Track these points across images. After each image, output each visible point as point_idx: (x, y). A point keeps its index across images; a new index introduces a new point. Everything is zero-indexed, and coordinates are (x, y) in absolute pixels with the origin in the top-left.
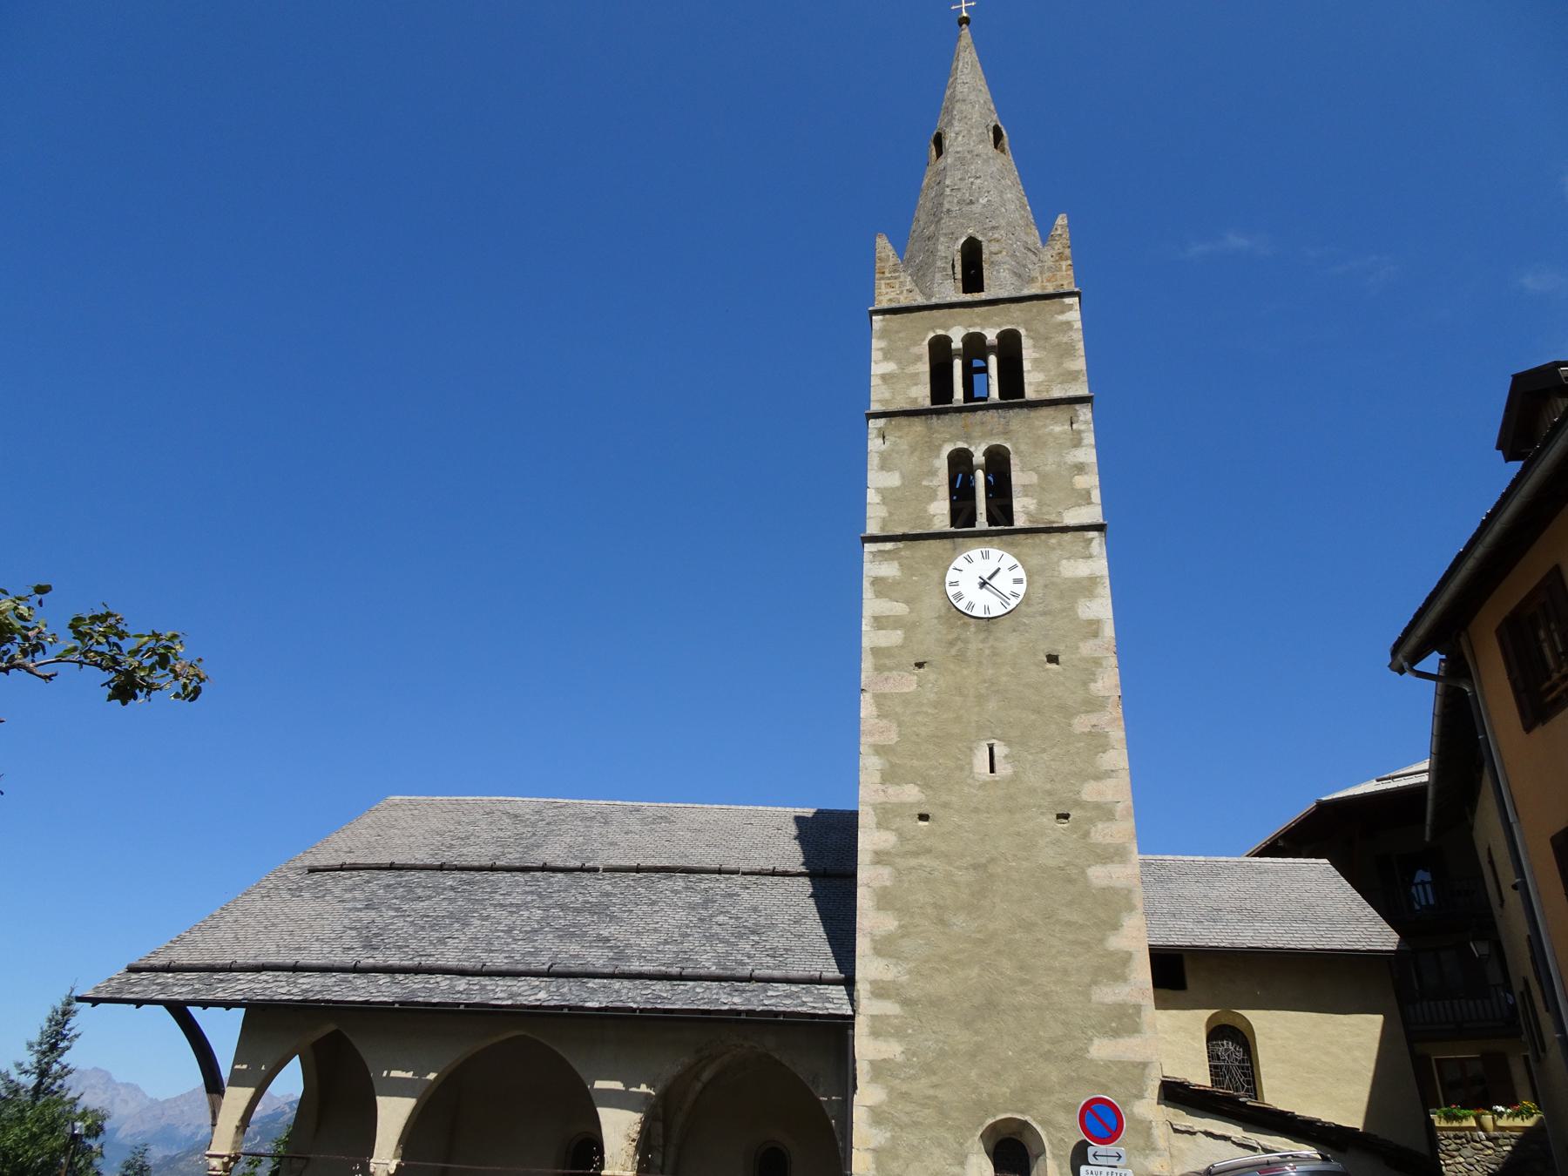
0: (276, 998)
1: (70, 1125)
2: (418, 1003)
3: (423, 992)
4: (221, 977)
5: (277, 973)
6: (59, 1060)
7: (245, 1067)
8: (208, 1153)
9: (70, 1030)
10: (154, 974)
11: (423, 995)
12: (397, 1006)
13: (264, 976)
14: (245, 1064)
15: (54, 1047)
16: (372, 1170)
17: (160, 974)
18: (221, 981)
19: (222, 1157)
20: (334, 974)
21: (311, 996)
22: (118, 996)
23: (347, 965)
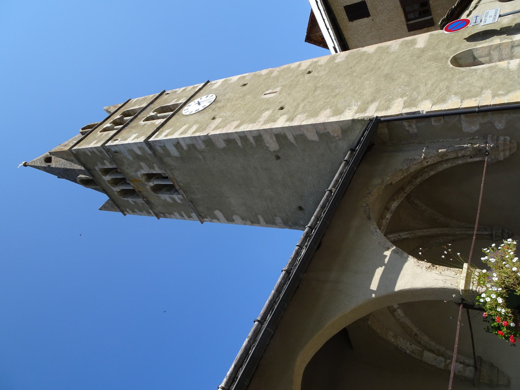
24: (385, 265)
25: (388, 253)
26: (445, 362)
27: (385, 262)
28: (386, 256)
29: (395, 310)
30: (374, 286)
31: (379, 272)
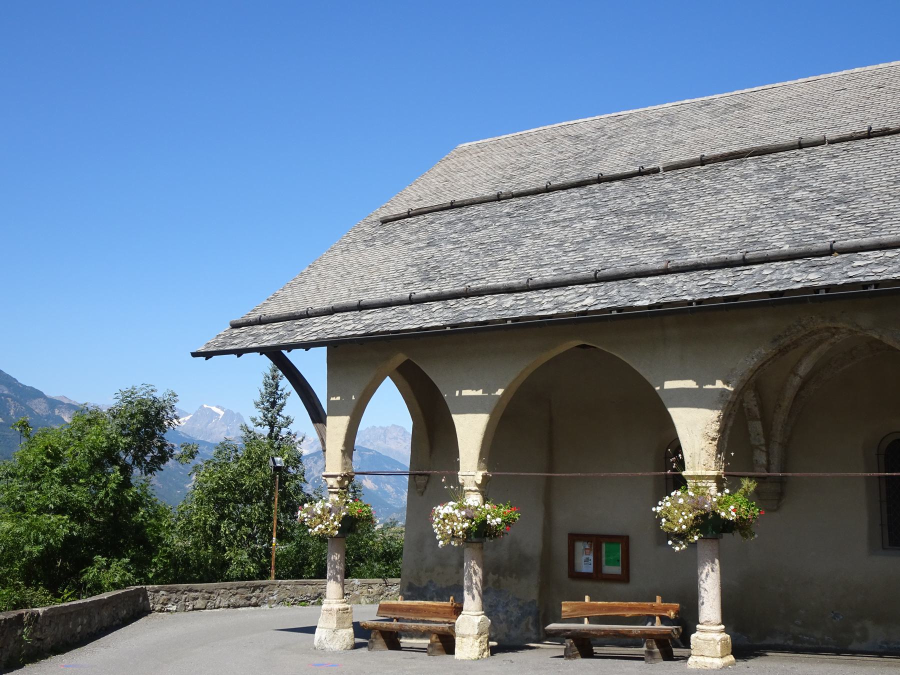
0: (343, 335)
2: (467, 324)
3: (472, 313)
4: (301, 323)
6: (280, 413)
7: (338, 398)
8: (324, 473)
9: (282, 390)
10: (251, 327)
11: (472, 316)
12: (448, 329)
13: (335, 318)
15: (273, 404)
16: (461, 481)
17: (255, 327)
18: (301, 326)
20: (393, 308)
21: (372, 330)
22: (221, 349)
24: (701, 387)
25: (719, 384)
26: (761, 445)
27: (705, 386)
28: (714, 384)
29: (796, 374)
30: (669, 385)
31: (690, 384)
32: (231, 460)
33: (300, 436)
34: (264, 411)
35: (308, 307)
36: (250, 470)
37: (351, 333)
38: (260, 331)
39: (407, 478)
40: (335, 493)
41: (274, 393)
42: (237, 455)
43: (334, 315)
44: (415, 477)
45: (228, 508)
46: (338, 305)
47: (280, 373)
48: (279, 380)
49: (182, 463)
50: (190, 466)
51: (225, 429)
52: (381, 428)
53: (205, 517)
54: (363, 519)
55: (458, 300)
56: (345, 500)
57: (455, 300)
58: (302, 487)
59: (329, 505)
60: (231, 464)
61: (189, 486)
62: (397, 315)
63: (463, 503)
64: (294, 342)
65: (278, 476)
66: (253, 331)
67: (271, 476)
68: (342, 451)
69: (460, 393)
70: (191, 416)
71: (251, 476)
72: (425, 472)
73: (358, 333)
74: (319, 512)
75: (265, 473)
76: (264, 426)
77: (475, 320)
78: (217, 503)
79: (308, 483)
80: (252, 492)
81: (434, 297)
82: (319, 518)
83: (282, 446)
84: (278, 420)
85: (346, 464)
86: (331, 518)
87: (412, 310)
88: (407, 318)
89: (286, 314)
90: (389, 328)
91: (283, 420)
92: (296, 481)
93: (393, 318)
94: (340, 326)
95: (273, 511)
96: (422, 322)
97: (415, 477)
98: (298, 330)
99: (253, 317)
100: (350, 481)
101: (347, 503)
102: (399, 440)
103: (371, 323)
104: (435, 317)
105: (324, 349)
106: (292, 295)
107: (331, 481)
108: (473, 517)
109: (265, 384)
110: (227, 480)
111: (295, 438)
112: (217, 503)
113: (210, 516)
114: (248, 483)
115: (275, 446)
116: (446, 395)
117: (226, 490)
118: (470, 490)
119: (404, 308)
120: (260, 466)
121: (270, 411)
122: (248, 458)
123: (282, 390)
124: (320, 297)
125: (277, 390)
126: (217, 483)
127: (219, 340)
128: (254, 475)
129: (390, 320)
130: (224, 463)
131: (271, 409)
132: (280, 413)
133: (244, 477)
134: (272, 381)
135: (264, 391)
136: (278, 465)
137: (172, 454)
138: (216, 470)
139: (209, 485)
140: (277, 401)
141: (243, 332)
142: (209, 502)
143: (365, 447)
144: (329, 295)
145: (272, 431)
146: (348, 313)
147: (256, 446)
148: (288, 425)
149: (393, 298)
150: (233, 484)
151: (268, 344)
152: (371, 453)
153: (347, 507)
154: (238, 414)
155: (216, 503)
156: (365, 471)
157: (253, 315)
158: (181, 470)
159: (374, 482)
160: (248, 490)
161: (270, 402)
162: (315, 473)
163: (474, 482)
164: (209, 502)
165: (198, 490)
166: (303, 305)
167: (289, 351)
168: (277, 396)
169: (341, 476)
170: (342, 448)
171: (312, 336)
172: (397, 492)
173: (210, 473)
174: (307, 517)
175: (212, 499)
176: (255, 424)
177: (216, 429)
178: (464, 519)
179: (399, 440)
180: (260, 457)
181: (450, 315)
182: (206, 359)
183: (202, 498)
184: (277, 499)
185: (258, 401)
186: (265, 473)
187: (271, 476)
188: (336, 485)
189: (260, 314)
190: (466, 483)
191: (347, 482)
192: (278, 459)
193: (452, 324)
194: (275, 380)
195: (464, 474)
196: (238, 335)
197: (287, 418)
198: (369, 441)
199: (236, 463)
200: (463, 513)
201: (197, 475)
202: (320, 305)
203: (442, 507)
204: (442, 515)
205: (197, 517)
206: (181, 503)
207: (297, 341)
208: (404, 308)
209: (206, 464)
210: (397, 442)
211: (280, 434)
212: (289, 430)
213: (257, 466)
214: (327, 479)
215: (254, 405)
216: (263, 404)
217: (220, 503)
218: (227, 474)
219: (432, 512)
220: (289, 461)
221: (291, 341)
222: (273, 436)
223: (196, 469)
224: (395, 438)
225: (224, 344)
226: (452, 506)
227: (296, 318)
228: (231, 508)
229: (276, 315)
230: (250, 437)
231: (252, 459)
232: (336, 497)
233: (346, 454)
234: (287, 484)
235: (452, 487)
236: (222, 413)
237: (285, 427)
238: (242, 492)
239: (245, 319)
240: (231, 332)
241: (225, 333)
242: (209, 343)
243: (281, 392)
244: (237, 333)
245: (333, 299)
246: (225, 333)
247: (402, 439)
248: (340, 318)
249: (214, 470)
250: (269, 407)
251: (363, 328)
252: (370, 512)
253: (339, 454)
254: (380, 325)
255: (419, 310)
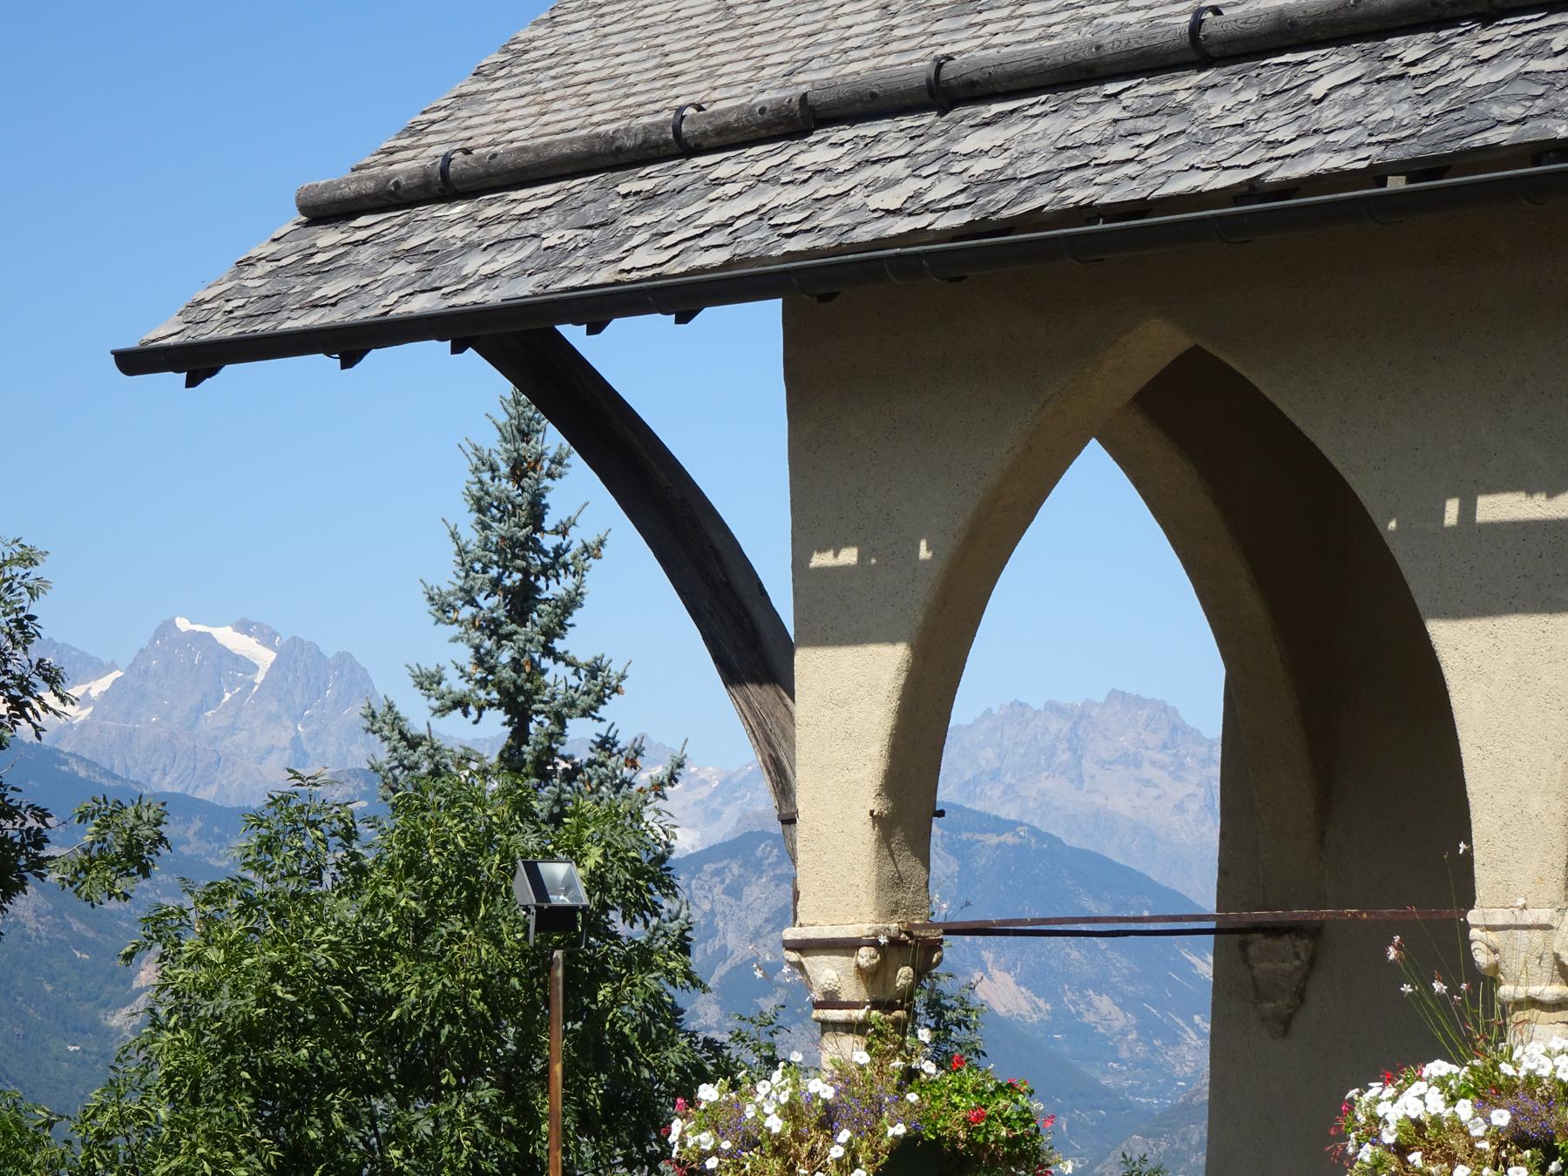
0: (863, 234)
1: (522, 879)
2: (1491, 155)
3: (1516, 99)
4: (647, 185)
5: (869, 130)
6: (559, 645)
7: (849, 556)
8: (790, 934)
9: (562, 531)
10: (400, 216)
11: (1516, 111)
12: (1396, 183)
13: (817, 152)
14: (847, 545)
15: (522, 601)
16: (1482, 958)
17: (423, 212)
18: (651, 199)
19: (846, 946)
20: (1111, 88)
21: (1007, 203)
22: (263, 327)
23: (1160, 37)
32: (327, 878)
33: (656, 763)
34: (476, 636)
35: (680, 102)
36: (422, 929)
37: (902, 225)
38: (449, 234)
39: (1201, 961)
40: (849, 1027)
41: (523, 545)
42: (355, 856)
43: (812, 139)
44: (1243, 946)
45: (325, 1115)
46: (829, 85)
47: (552, 439)
48: (547, 482)
49: (88, 899)
50: (136, 910)
51: (283, 737)
52: (1054, 708)
53: (214, 1162)
54: (993, 1158)
55: (1443, 34)
56: (898, 1063)
57: (1429, 35)
58: (677, 1011)
59: (821, 1088)
60: (328, 902)
61: (123, 1020)
62: (1129, 125)
63: (1495, 1065)
64: (617, 283)
65: (558, 954)
66: (410, 234)
67: (524, 956)
68: (876, 819)
69: (1468, 510)
70: (118, 674)
71: (429, 958)
72: (1299, 913)
73: (939, 225)
74: (775, 1124)
75: (496, 940)
76: (481, 709)
77: (1532, 132)
78: (271, 1093)
79: (706, 990)
80: (435, 1034)
81: (1316, 24)
82: (777, 1151)
83: (570, 807)
84: (548, 678)
85: (898, 882)
86: (837, 1152)
87: (1209, 96)
88: (1181, 141)
89: (571, 141)
90: (1092, 190)
91: (574, 681)
92: (649, 979)
93: (1111, 141)
94: (846, 193)
95: (544, 1127)
96: (1262, 153)
97: (1243, 946)
98: (638, 221)
99: (410, 164)
100: (923, 970)
101: (911, 1075)
102: (1148, 771)
103: (1001, 171)
104: (1325, 125)
105: (769, 312)
106: (599, 48)
107: (828, 972)
108: (1552, 1137)
109: (478, 500)
110: (310, 979)
111: (634, 766)
112: (271, 1093)
113: (239, 1157)
114: (412, 993)
115: (540, 807)
116: (1392, 525)
117: (306, 1029)
118: (1533, 1003)
119: (1167, 87)
120: (469, 908)
121: (509, 636)
122: (411, 867)
123: (562, 531)
124: (739, 49)
125: (539, 528)
126: (266, 997)
127: (249, 283)
128: (443, 952)
129: (1096, 151)
130: (295, 896)
131: (513, 627)
132: (559, 645)
133: (393, 964)
134: (509, 487)
135: (471, 536)
136: (560, 899)
137: (43, 854)
138: (256, 931)
139: (226, 1004)
140: (541, 583)
141: (364, 242)
142: (229, 1091)
143: (979, 806)
144: (783, 38)
145: (520, 734)
146: (883, 125)
147: (448, 808)
148: (601, 700)
149: (1106, 38)
150: (343, 999)
151: (491, 296)
152: (1008, 838)
153: (912, 1097)
154: (345, 659)
155: (262, 1094)
156: (991, 916)
157: (410, 154)
158: (82, 944)
159: (1032, 981)
160: (415, 1025)
161: (507, 591)
162: (732, 940)
163: (1548, 961)
164: (229, 1091)
165: (175, 1030)
166: (657, 95)
167: (594, 329)
168: (537, 561)
169: (875, 944)
170: (876, 806)
171: (707, 249)
172: (1148, 1028)
173: (227, 947)
174: (716, 1151)
175: (246, 1075)
176: (436, 704)
177: (242, 736)
178: (1503, 1144)
179: (1148, 771)
180: (465, 866)
181: (1403, 112)
182: (192, 382)
183: (194, 1071)
184: (558, 1069)
185: (446, 588)
186: (496, 940)
187: (524, 956)
188: (852, 990)
189: (442, 150)
190: (1513, 963)
191: (904, 975)
192: (556, 871)
193: (1415, 161)
194: (525, 482)
195: (1500, 921)
196: (341, 256)
197: (594, 670)
198: (995, 775)
199: (353, 891)
200: (1501, 1118)
201: (163, 958)
202: (738, 90)
203: (1390, 1091)
204: (1392, 1127)
205: (174, 1163)
206: (96, 1096)
207: (635, 275)
208: (1167, 87)
209: (207, 902)
210: (1138, 780)
211: (562, 750)
212: (602, 729)
213: (454, 909)
214: (809, 962)
215: (428, 606)
216: (472, 602)
217: (286, 1095)
218: (310, 948)
219: (1341, 1113)
220: (610, 878)
221: (603, 276)
222: (528, 758)
223: (160, 925)
224: (1130, 760)
225: (273, 303)
226: (1442, 1082)
227: (622, 159)
228: (336, 1118)
229: (524, 150)
230: (415, 766)
231: (424, 875)
232: (856, 1052)
233: (898, 837)
234: (604, 992)
235: (1438, 986)
236: (264, 657)
237: (585, 713)
238: (388, 1038)
239: (371, 178)
240: (305, 243)
241: (274, 247)
242: (200, 303)
243: (558, 539)
244: (334, 246)
245: (804, 55)
246: (274, 247)
247: (1163, 767)
248: (839, 151)
249: (248, 930)
250: (501, 614)
251: (960, 200)
252: (1027, 1122)
253: (864, 836)
254: (1045, 178)
255: (1243, 96)
